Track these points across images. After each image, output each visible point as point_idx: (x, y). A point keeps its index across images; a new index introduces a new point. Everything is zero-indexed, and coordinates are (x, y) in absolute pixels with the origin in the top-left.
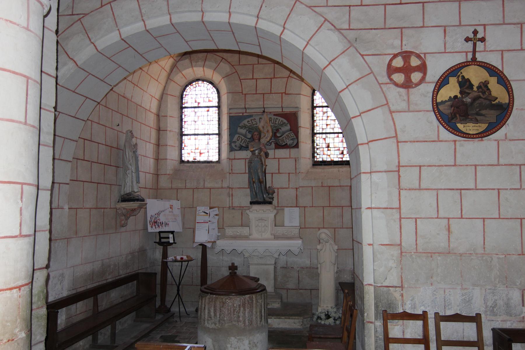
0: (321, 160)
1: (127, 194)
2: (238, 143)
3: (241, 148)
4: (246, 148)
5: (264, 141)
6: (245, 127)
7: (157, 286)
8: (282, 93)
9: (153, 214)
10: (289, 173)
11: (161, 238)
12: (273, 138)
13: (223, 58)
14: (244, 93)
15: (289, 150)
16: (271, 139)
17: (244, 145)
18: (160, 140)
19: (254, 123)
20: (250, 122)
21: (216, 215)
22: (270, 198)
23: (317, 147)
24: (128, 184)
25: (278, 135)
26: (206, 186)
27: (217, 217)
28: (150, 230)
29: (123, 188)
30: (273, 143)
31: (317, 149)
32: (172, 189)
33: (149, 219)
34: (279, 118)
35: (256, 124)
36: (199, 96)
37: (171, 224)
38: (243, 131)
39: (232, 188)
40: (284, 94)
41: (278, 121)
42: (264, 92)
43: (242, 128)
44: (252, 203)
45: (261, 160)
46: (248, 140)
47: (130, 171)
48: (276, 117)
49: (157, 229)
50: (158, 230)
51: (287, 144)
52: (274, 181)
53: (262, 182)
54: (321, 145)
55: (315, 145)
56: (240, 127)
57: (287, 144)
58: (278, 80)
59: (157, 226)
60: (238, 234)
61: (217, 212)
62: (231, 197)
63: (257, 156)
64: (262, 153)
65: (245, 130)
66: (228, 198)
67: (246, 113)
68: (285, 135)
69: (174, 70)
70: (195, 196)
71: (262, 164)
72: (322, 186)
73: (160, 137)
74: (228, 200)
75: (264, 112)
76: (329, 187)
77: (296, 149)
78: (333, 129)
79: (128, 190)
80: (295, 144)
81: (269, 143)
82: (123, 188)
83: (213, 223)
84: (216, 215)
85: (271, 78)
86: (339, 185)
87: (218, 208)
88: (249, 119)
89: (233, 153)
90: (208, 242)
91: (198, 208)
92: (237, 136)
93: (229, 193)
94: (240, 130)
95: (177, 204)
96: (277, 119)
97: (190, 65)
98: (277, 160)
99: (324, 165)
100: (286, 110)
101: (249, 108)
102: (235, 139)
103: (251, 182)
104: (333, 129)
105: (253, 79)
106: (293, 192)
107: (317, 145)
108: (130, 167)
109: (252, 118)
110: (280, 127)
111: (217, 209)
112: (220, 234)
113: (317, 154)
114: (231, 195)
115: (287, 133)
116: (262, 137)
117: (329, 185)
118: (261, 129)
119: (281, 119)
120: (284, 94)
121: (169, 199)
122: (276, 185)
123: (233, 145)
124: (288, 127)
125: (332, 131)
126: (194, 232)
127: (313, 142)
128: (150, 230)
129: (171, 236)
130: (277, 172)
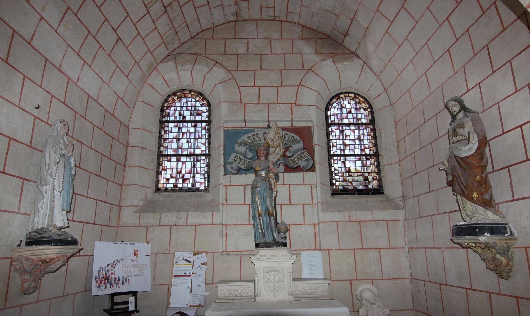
0: (341, 187)
1: (37, 231)
2: (235, 165)
3: (239, 171)
4: (249, 169)
5: (273, 158)
6: (244, 143)
7: (175, 214)
8: (292, 104)
9: (104, 265)
10: (304, 204)
11: (113, 304)
12: (281, 159)
13: (217, 62)
14: (243, 102)
15: (302, 173)
16: (278, 160)
17: (243, 167)
18: (127, 160)
19: (256, 139)
20: (252, 138)
21: (203, 264)
22: (282, 238)
23: (336, 172)
24: (42, 211)
25: (288, 154)
26: (189, 222)
27: (204, 267)
28: (95, 291)
29: (32, 219)
30: (281, 165)
31: (336, 174)
32: (139, 226)
33: (95, 273)
34: (289, 133)
35: (260, 140)
36: (185, 108)
37: (132, 280)
38: (242, 149)
39: (226, 225)
40: (294, 105)
41: (287, 136)
42: (268, 103)
43: (240, 145)
44: (257, 246)
45: (270, 185)
46: (248, 160)
47: (50, 187)
48: (284, 132)
49: (109, 289)
50: (110, 291)
51: (299, 166)
52: (287, 215)
53: (272, 214)
54: (340, 169)
55: (333, 170)
56: (238, 143)
57: (299, 166)
58: (286, 88)
59: (108, 285)
60: (236, 293)
61: (205, 260)
62: (224, 238)
63: (265, 179)
64: (271, 175)
65: (245, 148)
66: (221, 239)
67: (245, 127)
68: (297, 155)
69: (153, 73)
70: (173, 237)
71: (271, 189)
72: (350, 221)
73: (128, 155)
74: (220, 242)
75: (269, 126)
76: (360, 221)
77: (312, 173)
78: (353, 150)
79: (40, 221)
80: (310, 166)
81: (276, 164)
82: (32, 219)
83: (198, 276)
84: (203, 264)
85: (278, 87)
86: (372, 219)
87: (207, 253)
88: (250, 135)
89: (228, 176)
90: (191, 306)
91: (177, 254)
92: (233, 155)
93: (222, 231)
94: (238, 148)
95: (145, 249)
96: (286, 134)
97: (175, 68)
98: (288, 186)
99: (346, 194)
100: (296, 125)
101: (250, 121)
102: (231, 159)
103: (256, 215)
104: (353, 150)
105: (255, 86)
106: (310, 230)
107: (335, 170)
108: (50, 180)
109: (255, 133)
110: (291, 144)
111: (204, 254)
112: (208, 293)
113: (337, 181)
114: (224, 235)
115: (299, 153)
116: (270, 152)
117: (359, 219)
118: (270, 142)
119: (292, 135)
120: (294, 105)
121: (133, 241)
122: (287, 221)
123: (229, 167)
124: (301, 145)
125: (352, 153)
126: (169, 291)
127: (330, 165)
128: (95, 291)
129: (131, 299)
130: (288, 202)
